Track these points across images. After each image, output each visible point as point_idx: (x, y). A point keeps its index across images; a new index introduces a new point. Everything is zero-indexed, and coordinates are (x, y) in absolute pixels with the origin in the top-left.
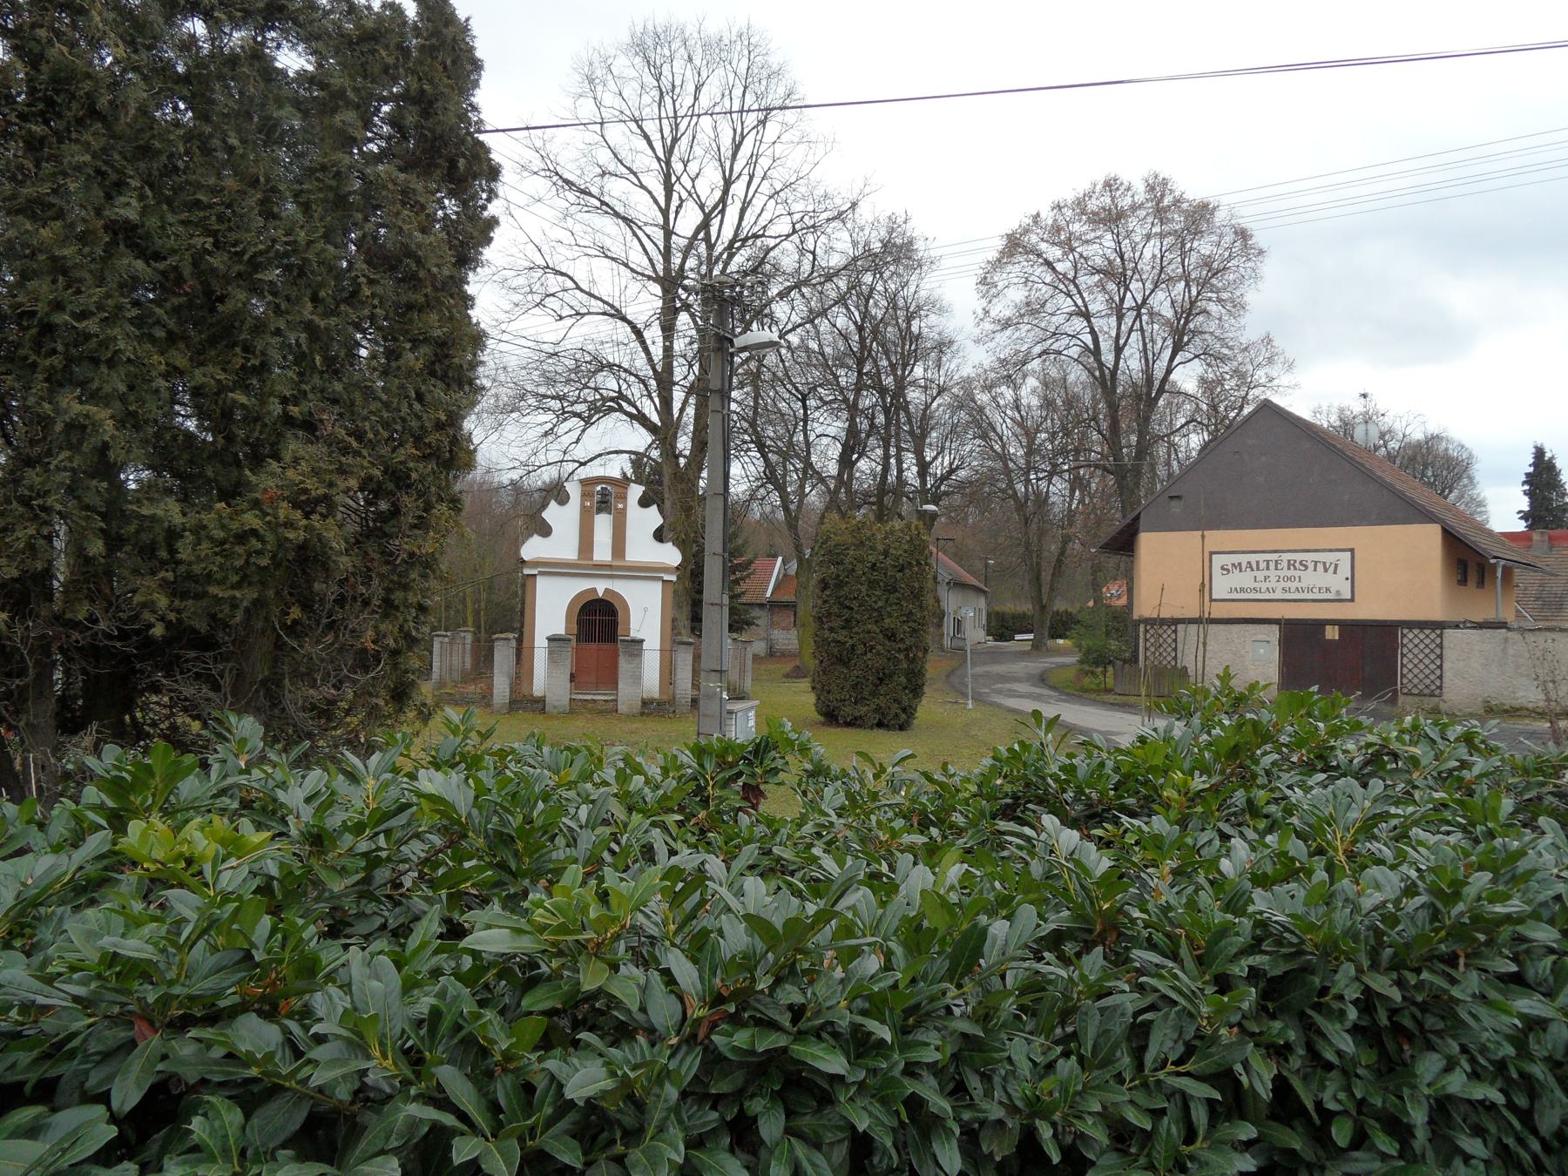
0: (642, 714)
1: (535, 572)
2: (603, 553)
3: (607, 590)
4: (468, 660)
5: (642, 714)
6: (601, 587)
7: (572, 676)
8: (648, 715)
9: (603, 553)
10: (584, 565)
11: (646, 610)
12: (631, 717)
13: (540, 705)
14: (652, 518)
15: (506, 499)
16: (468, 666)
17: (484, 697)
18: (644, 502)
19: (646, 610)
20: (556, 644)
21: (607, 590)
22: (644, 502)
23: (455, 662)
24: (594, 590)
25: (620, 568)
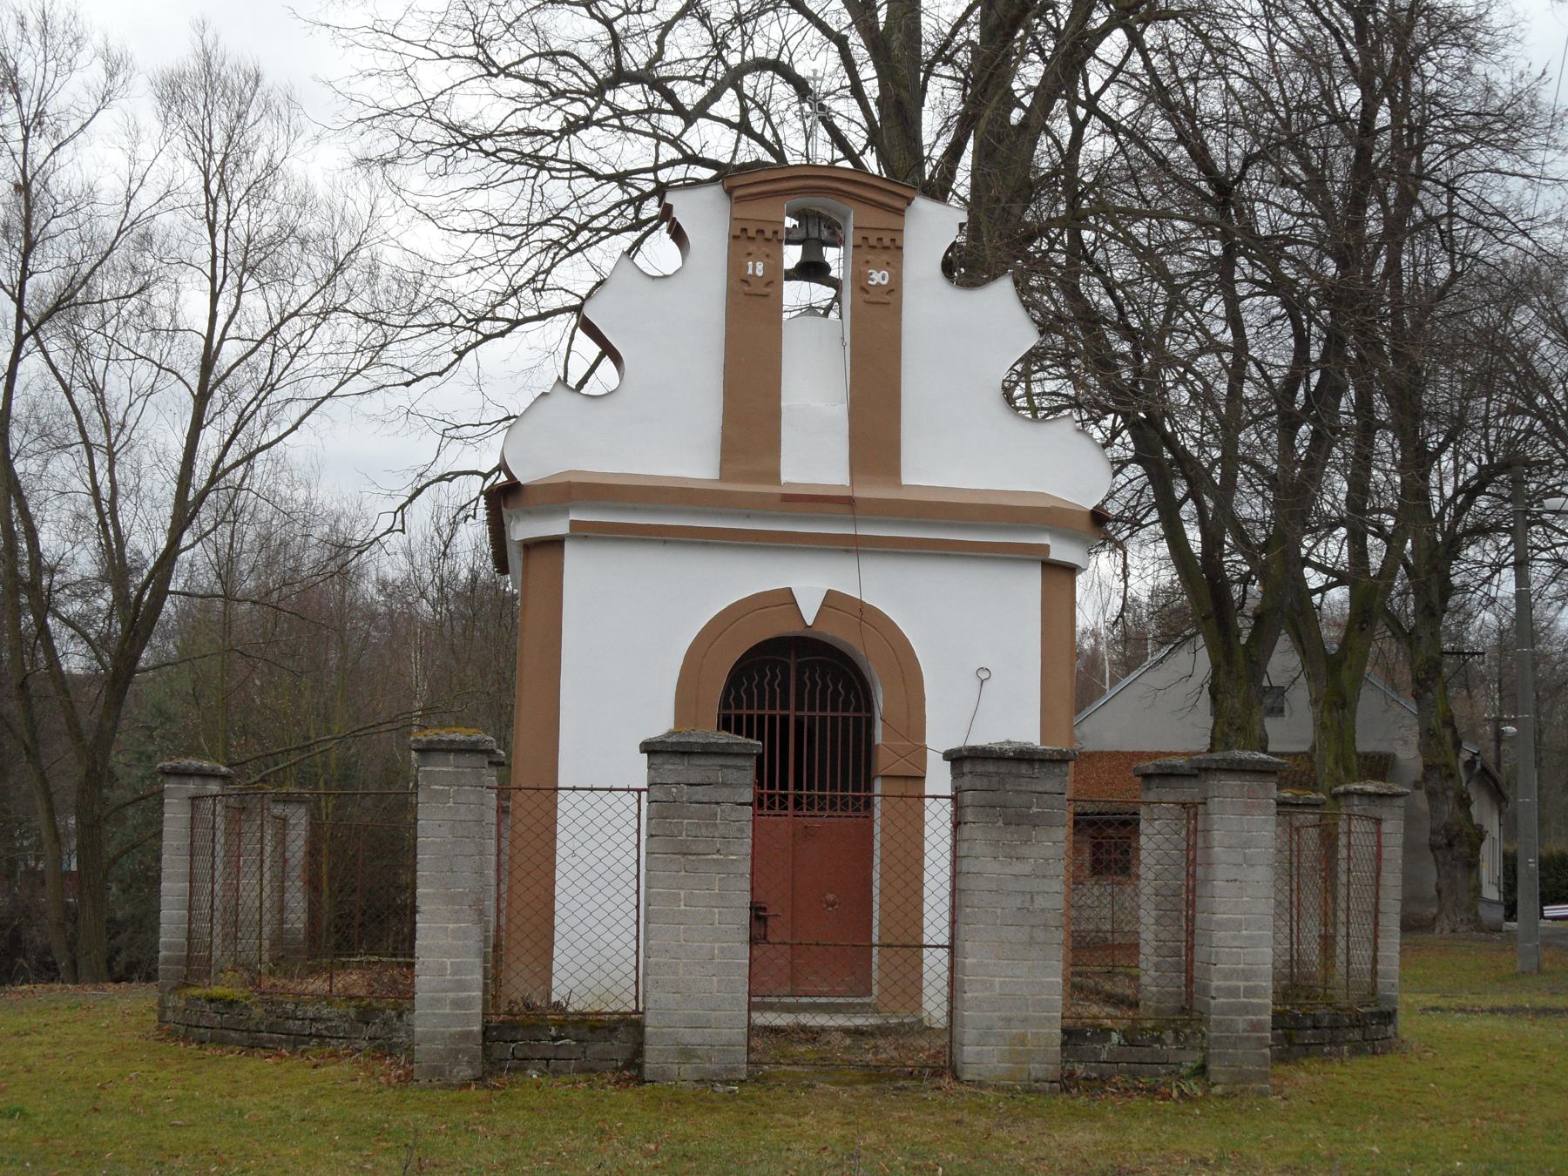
0: (1067, 1082)
1: (557, 527)
2: (814, 453)
3: (833, 601)
4: (297, 901)
5: (1067, 1082)
6: (810, 584)
7: (758, 914)
8: (1096, 1085)
9: (814, 453)
10: (741, 502)
11: (983, 676)
12: (1020, 1095)
13: (618, 1048)
14: (998, 321)
15: (404, 879)
16: (297, 919)
17: (365, 1016)
18: (965, 267)
19: (983, 676)
20: (675, 769)
21: (833, 601)
22: (965, 267)
23: (249, 896)
24: (785, 599)
25: (880, 513)
